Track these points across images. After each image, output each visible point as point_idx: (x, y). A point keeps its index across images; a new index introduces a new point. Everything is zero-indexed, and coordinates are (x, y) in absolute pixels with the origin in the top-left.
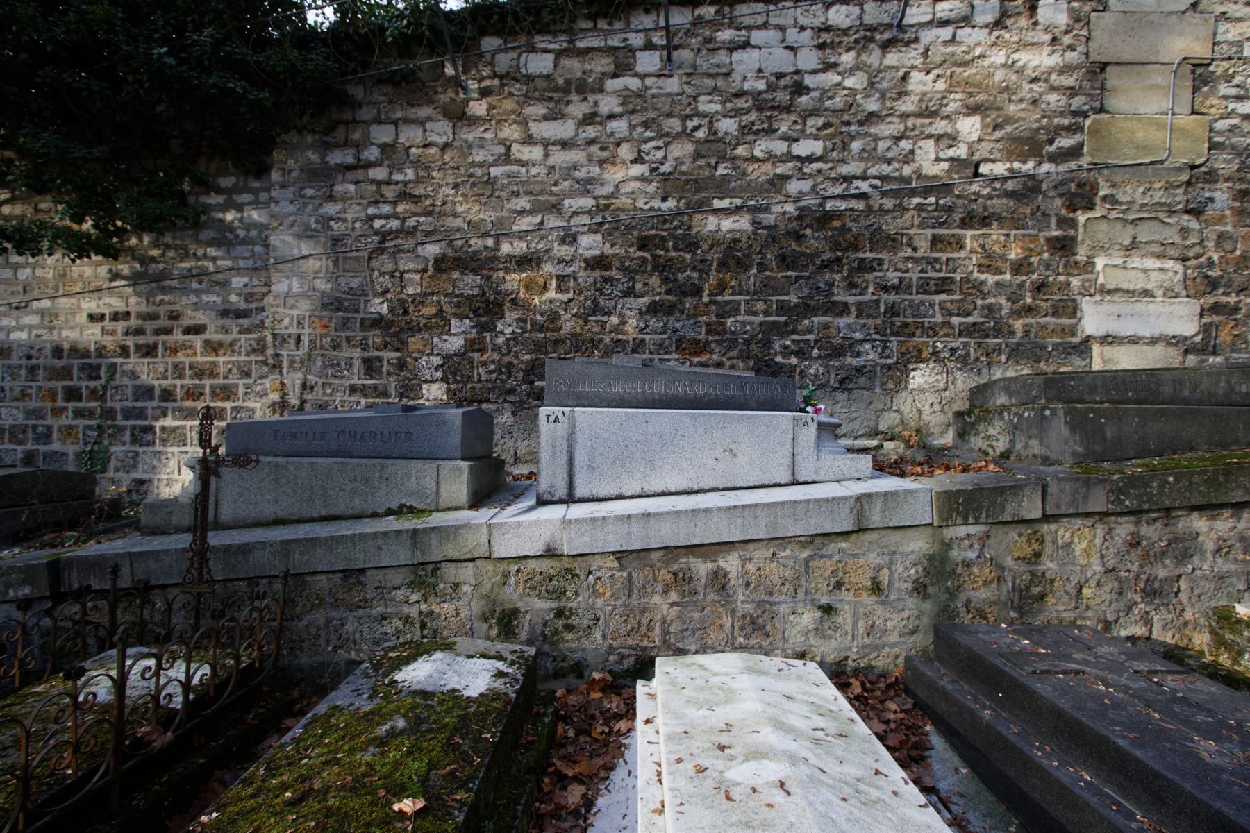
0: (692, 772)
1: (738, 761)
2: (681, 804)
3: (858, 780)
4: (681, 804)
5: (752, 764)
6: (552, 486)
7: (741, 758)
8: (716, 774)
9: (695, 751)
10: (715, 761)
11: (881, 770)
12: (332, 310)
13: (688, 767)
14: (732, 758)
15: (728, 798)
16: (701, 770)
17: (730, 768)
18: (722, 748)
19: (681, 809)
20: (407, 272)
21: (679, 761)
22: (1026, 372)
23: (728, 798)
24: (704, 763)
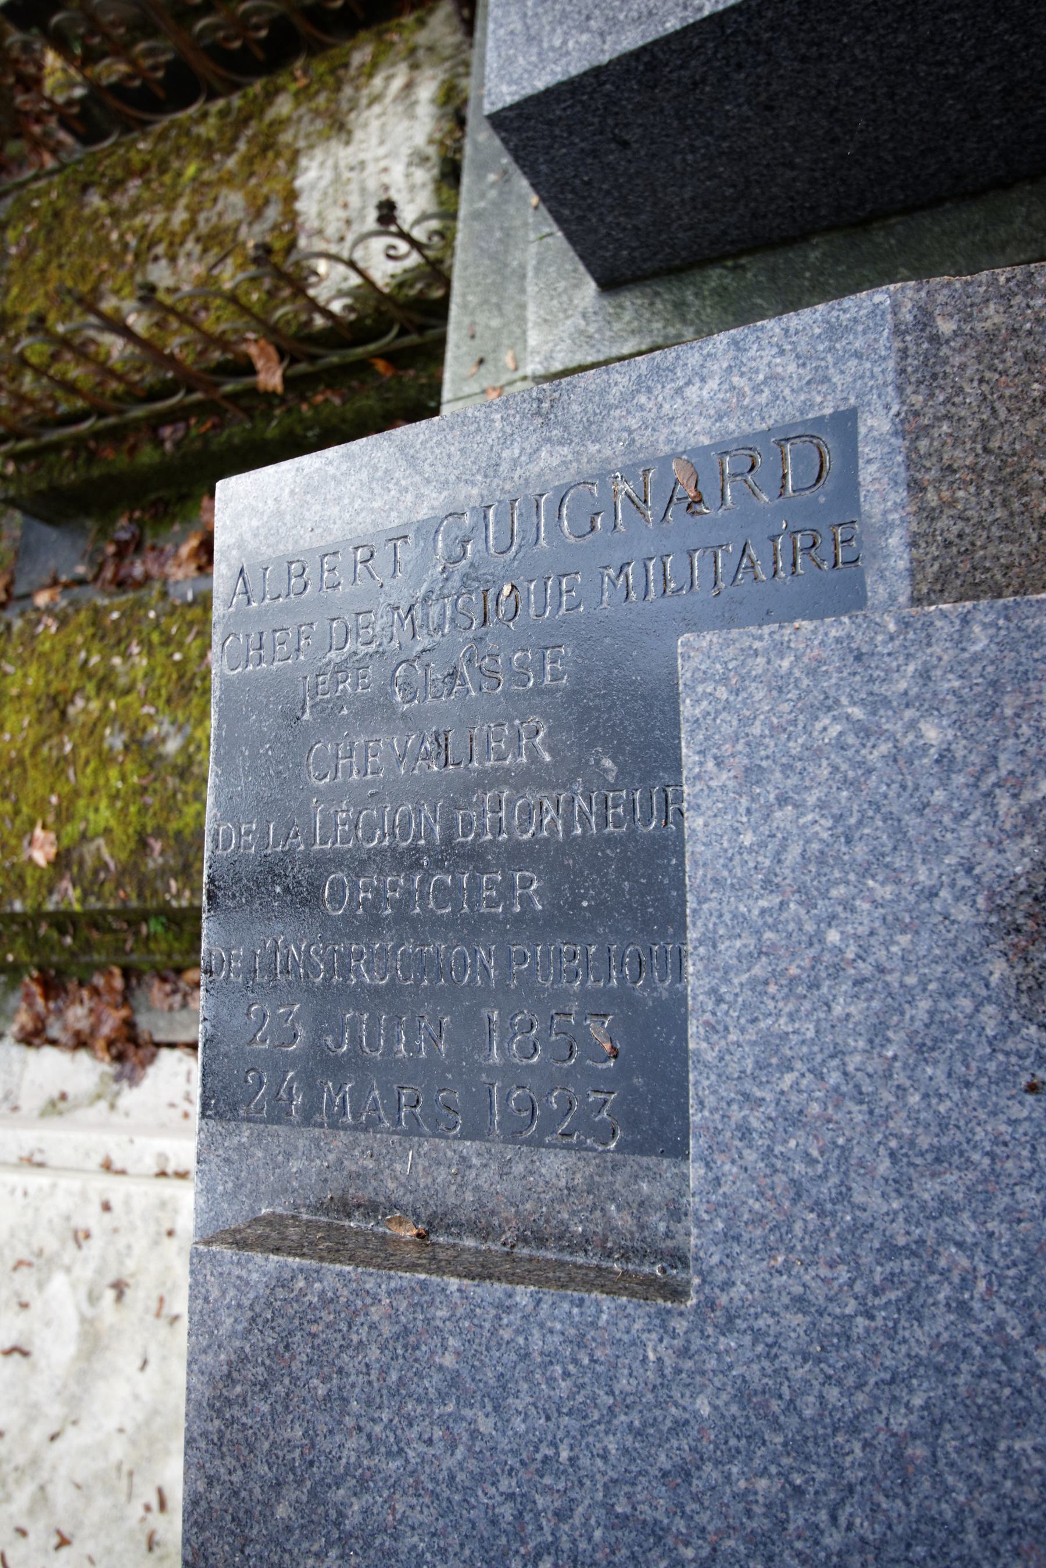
0: (80, 1222)
1: (85, 1306)
2: (25, 1194)
3: (42, 1488)
4: (25, 1194)
5: (72, 1326)
6: (386, 188)
7: (89, 1312)
8: (66, 1259)
9: (122, 1241)
10: (92, 1265)
11: (65, 1551)
12: (1016, 593)
13: (92, 1218)
14: (93, 1298)
15: (19, 1264)
16: (81, 1237)
17: (74, 1286)
18: (119, 1288)
19: (19, 1193)
20: (510, 669)
21: (106, 1207)
22: (29, 229)
23: (19, 1264)
24: (94, 1248)
